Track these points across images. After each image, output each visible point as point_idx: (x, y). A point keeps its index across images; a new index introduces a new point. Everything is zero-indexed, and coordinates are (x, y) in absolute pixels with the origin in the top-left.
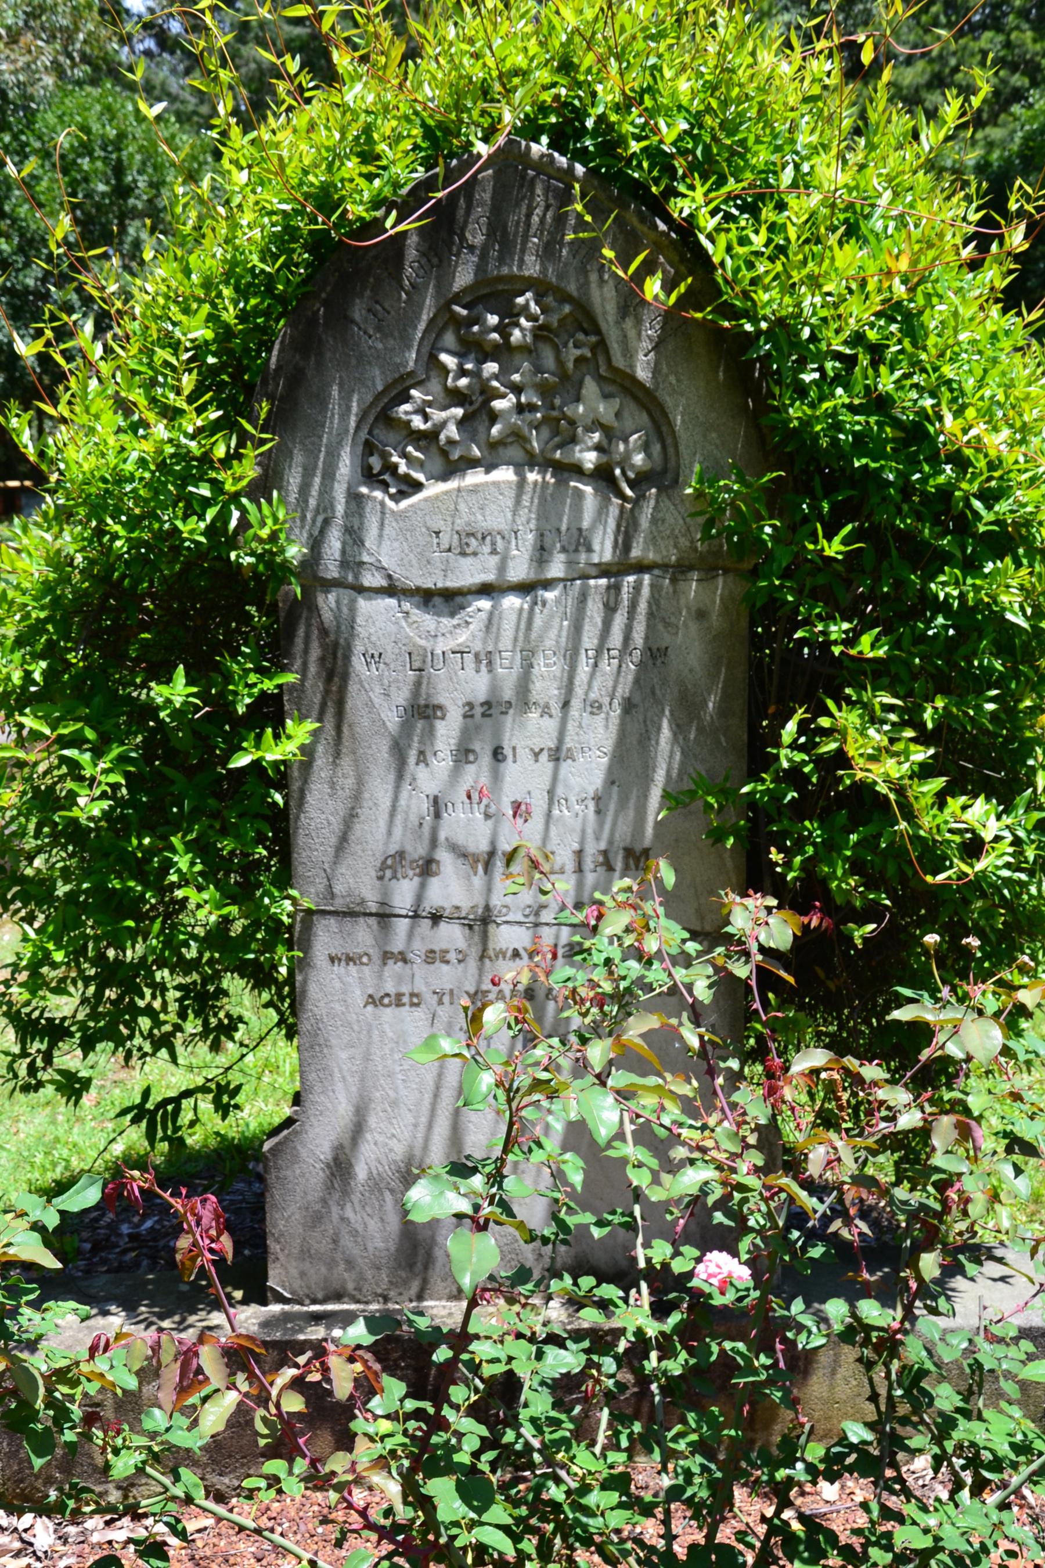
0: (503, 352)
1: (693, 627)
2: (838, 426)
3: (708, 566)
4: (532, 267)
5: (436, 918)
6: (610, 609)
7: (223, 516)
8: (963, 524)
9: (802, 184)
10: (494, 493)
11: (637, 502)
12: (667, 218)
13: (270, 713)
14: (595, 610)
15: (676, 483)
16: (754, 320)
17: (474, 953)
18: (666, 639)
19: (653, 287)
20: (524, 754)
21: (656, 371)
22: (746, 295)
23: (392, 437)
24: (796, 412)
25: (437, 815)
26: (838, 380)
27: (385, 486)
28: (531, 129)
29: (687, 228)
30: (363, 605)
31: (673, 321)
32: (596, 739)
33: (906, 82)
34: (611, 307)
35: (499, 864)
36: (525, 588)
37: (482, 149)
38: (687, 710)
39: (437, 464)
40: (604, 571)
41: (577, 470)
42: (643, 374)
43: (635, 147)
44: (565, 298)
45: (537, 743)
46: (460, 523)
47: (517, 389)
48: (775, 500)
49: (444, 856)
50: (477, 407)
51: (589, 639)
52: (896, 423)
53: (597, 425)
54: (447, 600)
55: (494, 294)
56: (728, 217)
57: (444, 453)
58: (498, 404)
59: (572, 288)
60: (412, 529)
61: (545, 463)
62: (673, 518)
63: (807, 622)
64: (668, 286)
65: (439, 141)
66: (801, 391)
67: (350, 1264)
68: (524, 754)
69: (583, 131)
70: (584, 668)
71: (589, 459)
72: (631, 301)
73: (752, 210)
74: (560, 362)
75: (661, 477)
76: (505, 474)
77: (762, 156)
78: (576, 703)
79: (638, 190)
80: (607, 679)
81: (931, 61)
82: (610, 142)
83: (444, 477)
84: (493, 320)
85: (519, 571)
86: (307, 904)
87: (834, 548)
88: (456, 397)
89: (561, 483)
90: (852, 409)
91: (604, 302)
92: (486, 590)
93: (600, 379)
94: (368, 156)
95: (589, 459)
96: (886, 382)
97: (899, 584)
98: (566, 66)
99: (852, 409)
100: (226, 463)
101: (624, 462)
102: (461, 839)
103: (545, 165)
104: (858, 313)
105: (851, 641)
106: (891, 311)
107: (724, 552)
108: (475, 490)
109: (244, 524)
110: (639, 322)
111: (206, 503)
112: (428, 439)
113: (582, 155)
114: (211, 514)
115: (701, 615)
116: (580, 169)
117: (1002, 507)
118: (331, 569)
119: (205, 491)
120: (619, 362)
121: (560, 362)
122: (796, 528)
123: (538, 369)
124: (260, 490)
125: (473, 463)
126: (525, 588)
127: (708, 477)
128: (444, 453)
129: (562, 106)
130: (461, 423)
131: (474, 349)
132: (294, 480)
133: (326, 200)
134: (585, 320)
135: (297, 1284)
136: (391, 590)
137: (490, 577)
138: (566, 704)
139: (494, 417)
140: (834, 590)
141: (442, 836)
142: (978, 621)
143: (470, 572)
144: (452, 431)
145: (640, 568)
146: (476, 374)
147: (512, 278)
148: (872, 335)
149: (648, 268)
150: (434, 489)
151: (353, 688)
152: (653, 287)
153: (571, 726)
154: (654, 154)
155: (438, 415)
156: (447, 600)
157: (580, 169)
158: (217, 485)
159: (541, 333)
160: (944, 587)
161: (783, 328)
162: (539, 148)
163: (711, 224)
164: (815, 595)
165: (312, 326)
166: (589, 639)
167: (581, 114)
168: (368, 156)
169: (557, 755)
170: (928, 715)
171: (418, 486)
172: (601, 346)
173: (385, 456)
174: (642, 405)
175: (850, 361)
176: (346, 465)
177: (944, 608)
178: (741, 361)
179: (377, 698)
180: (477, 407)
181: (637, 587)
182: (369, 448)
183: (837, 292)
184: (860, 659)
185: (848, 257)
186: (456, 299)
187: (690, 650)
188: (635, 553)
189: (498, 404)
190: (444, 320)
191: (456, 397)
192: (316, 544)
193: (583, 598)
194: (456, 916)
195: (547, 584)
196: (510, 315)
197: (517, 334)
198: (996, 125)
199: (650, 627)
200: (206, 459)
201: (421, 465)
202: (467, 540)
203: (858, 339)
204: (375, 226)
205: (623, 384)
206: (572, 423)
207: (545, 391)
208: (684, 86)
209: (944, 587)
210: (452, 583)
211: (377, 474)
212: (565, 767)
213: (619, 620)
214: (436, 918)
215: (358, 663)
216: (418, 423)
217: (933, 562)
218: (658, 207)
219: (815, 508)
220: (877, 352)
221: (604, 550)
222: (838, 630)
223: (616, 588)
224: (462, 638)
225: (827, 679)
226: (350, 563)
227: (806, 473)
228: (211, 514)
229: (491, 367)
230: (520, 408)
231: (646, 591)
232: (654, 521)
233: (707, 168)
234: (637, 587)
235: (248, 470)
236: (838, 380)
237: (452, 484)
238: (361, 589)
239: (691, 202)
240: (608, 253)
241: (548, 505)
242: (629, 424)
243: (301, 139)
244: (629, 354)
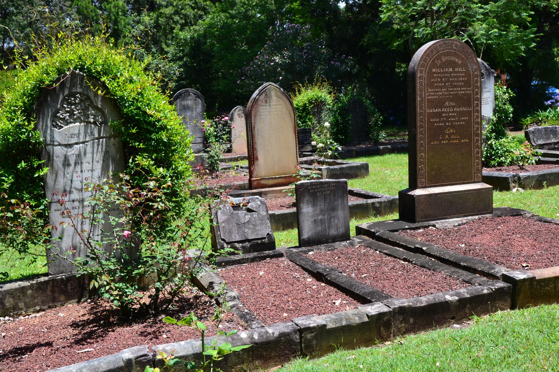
0: (75, 104)
1: (113, 147)
2: (132, 112)
3: (115, 137)
4: (79, 90)
5: (73, 201)
6: (98, 145)
7: (29, 135)
8: (154, 125)
9: (121, 75)
10: (76, 127)
11: (101, 127)
12: (100, 81)
13: (40, 167)
14: (96, 145)
15: (107, 123)
16: (117, 96)
17: (81, 207)
18: (109, 149)
19: (100, 92)
20: (86, 171)
21: (101, 105)
22: (115, 93)
23: (57, 119)
24: (125, 110)
25: (72, 183)
26: (131, 105)
27: (56, 128)
28: (75, 68)
29: (104, 83)
30: (55, 148)
31: (103, 97)
32: (98, 167)
33: (168, 12)
34: (93, 96)
35: (83, 190)
36: (83, 143)
37: (68, 73)
38: (113, 160)
39: (65, 123)
40: (97, 139)
41: (90, 122)
42: (100, 106)
43: (94, 71)
44: (85, 95)
45: (88, 169)
46: (70, 133)
47: (78, 110)
48: (124, 124)
49: (73, 190)
50: (71, 113)
51: (95, 151)
52: (142, 111)
53: (92, 115)
54: (70, 146)
55: (73, 95)
56: (110, 81)
57: (66, 121)
58: (75, 113)
59: (86, 93)
60: (59, 135)
61: (84, 122)
62: (107, 129)
63: (131, 143)
64: (102, 92)
65: (60, 72)
66: (126, 107)
67: (64, 266)
68: (86, 171)
69: (84, 69)
70: (95, 155)
71: (92, 120)
72: (96, 94)
73: (114, 79)
74: (85, 105)
75: (105, 122)
76: (78, 124)
77: (115, 71)
78: (94, 161)
79: (95, 77)
80: (99, 157)
81: (174, 7)
82: (89, 70)
83: (67, 125)
84: (73, 99)
85: (81, 140)
86: (49, 201)
87: (134, 131)
88: (67, 112)
89: (87, 125)
90: (135, 109)
91: (91, 95)
92: (76, 144)
93: (92, 107)
94: (48, 74)
95: (92, 120)
96: (139, 105)
97: (146, 136)
98: (80, 58)
99: (135, 109)
100: (28, 126)
101: (98, 121)
102: (77, 187)
103: (78, 74)
104: (133, 95)
105: (139, 145)
106: (139, 94)
107: (117, 133)
108: (73, 127)
109: (32, 135)
110: (98, 98)
111: (25, 132)
112: (63, 119)
113: (85, 72)
114: (26, 134)
115: (114, 145)
116: (85, 74)
117: (160, 123)
118: (48, 142)
119: (24, 130)
120: (95, 104)
121: (85, 105)
122: (128, 129)
123: (81, 106)
124: (35, 129)
125: (71, 123)
126: (83, 143)
127: (113, 121)
128: (66, 121)
129: (81, 65)
130: (69, 116)
131: (70, 104)
132: (40, 127)
133: (42, 81)
134: (88, 98)
135: (54, 271)
136: (60, 145)
137: (76, 141)
138: (93, 162)
139: (75, 115)
140: (136, 137)
141: (73, 186)
142: (159, 141)
143: (73, 141)
144: (68, 117)
145: (103, 138)
146: (70, 108)
147: (75, 92)
148: (136, 98)
149: (98, 89)
150: (65, 127)
151: (54, 162)
152: (100, 92)
153: (94, 166)
154: (97, 72)
155: (65, 115)
156: (70, 146)
157: (85, 74)
158: (27, 130)
159: (81, 100)
160: (153, 136)
161: (122, 98)
162: (78, 71)
163: (108, 82)
164: (132, 139)
165: (40, 101)
166: (95, 151)
167: (84, 66)
168: (48, 74)
169: (92, 170)
170: (153, 157)
171: (62, 127)
172: (92, 102)
173: (56, 122)
174: (100, 111)
175: (133, 102)
176: (49, 124)
177: (154, 140)
178: (115, 103)
179: (58, 162)
180: (71, 113)
181: (103, 141)
182: (53, 121)
183: (129, 92)
184: (140, 148)
185: (130, 86)
186: (66, 96)
187: (113, 151)
188: (102, 135)
189: (75, 113)
190: (64, 100)
191: (67, 112)
192: (45, 137)
193: (93, 144)
194: (77, 200)
195: (87, 142)
196: (76, 98)
197: (77, 101)
198: (196, 25)
199: (106, 148)
200: (24, 125)
201: (62, 123)
202: (72, 136)
203: (134, 98)
204: (52, 85)
205: (96, 108)
206: (88, 115)
207: (83, 110)
208: (100, 61)
209: (153, 136)
210: (70, 143)
211: (56, 126)
212: (94, 172)
213: (100, 147)
214: (73, 201)
215: (55, 158)
216: (61, 116)
217: (151, 133)
218: (99, 80)
219: (131, 125)
220: (137, 100)
221: (96, 135)
222: (137, 144)
223: (99, 141)
224: (73, 152)
225: (136, 152)
226: (52, 141)
227: (129, 120)
228: (26, 134)
229: (73, 107)
230: (79, 113)
231: (104, 141)
232: (104, 130)
233: (106, 74)
234: (103, 141)
235: (32, 126)
236: (131, 105)
237: (68, 126)
238: (54, 145)
239: (104, 79)
240: (92, 87)
241: (86, 127)
242: (98, 114)
243: (34, 71)
244: (96, 103)
